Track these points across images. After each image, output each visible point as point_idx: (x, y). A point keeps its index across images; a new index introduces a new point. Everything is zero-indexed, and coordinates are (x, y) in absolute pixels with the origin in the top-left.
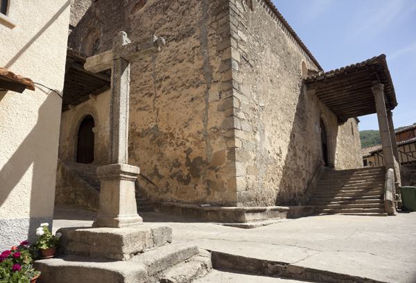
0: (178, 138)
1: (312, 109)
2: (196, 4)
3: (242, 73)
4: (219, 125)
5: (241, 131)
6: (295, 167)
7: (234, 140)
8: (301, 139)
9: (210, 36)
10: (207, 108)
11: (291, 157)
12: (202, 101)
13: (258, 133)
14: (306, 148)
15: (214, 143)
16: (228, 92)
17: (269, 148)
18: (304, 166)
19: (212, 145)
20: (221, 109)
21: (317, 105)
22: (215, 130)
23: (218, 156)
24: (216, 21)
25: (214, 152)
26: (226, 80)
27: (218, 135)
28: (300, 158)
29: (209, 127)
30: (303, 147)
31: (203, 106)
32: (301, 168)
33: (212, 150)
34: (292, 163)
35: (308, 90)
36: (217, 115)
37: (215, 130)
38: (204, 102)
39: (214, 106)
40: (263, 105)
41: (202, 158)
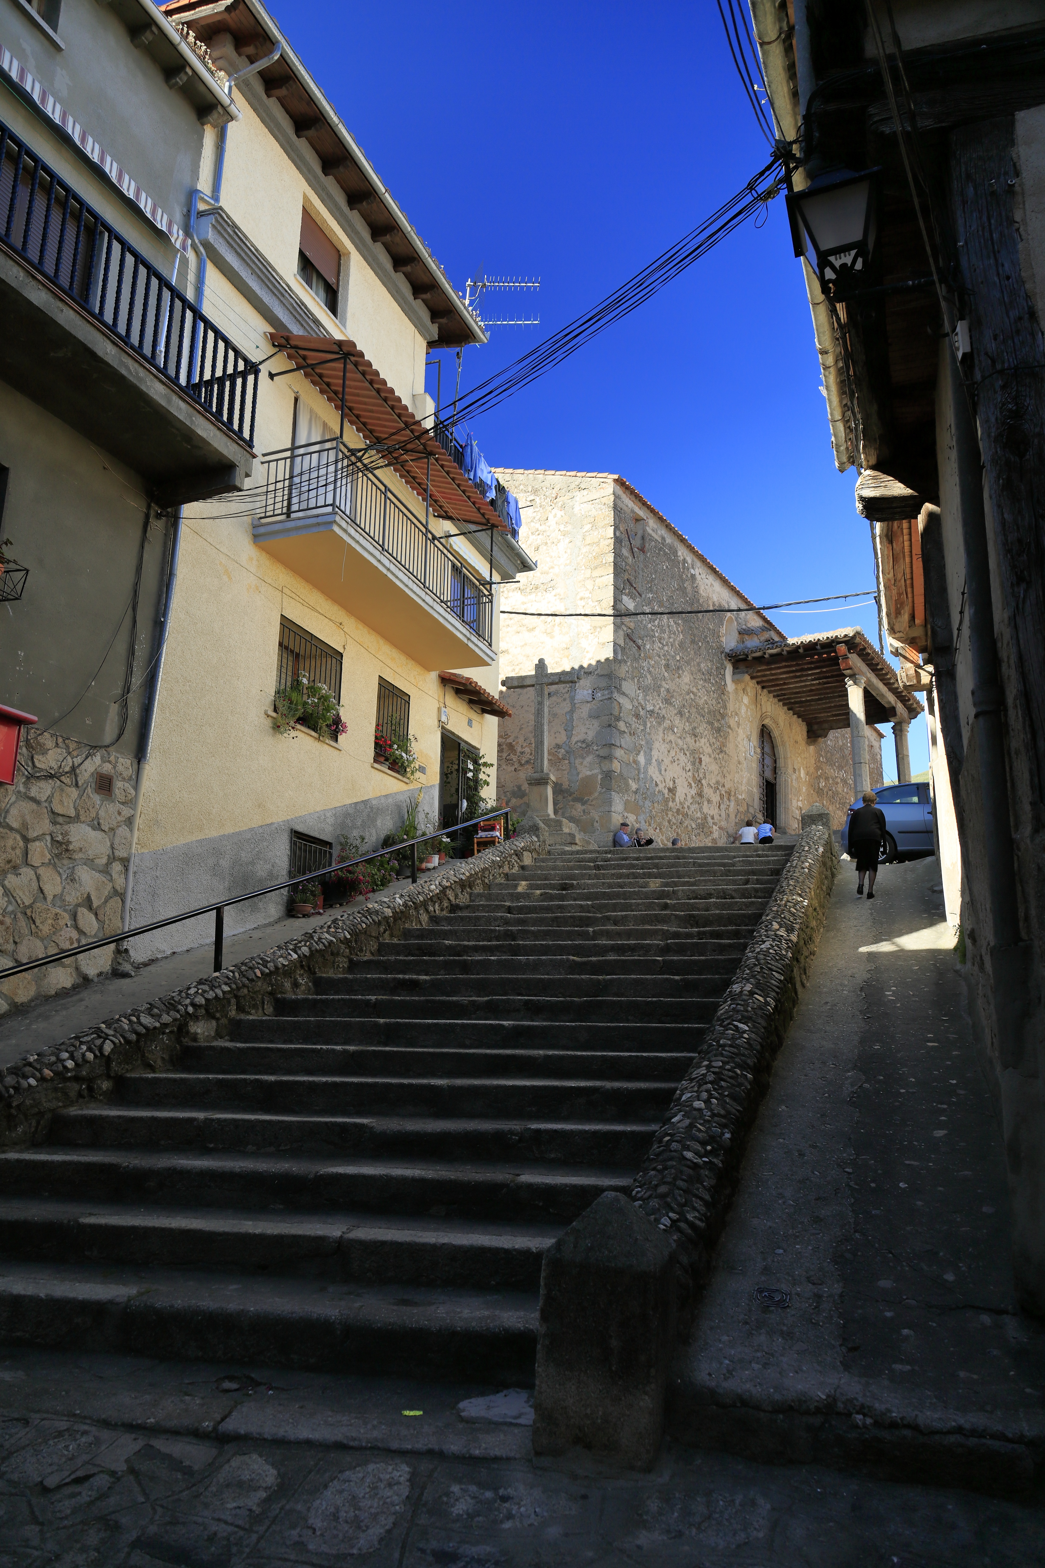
0: (522, 753)
1: (743, 710)
2: (559, 541)
3: (626, 662)
4: (590, 739)
5: (619, 750)
6: (699, 815)
7: (611, 761)
8: (714, 767)
9: (581, 599)
10: (572, 712)
11: (693, 797)
12: (565, 700)
13: (642, 753)
14: (724, 786)
15: (582, 763)
16: (606, 692)
17: (657, 777)
18: (716, 817)
19: (578, 766)
20: (594, 716)
21: (756, 701)
22: (584, 746)
23: (587, 783)
24: (591, 577)
25: (580, 776)
26: (602, 673)
27: (588, 753)
28: (709, 801)
29: (574, 739)
30: (718, 782)
31: (566, 707)
32: (709, 819)
33: (578, 774)
34: (693, 808)
35: (734, 673)
36: (587, 723)
37: (584, 746)
38: (568, 701)
39: (584, 711)
40: (652, 708)
41: (562, 785)
